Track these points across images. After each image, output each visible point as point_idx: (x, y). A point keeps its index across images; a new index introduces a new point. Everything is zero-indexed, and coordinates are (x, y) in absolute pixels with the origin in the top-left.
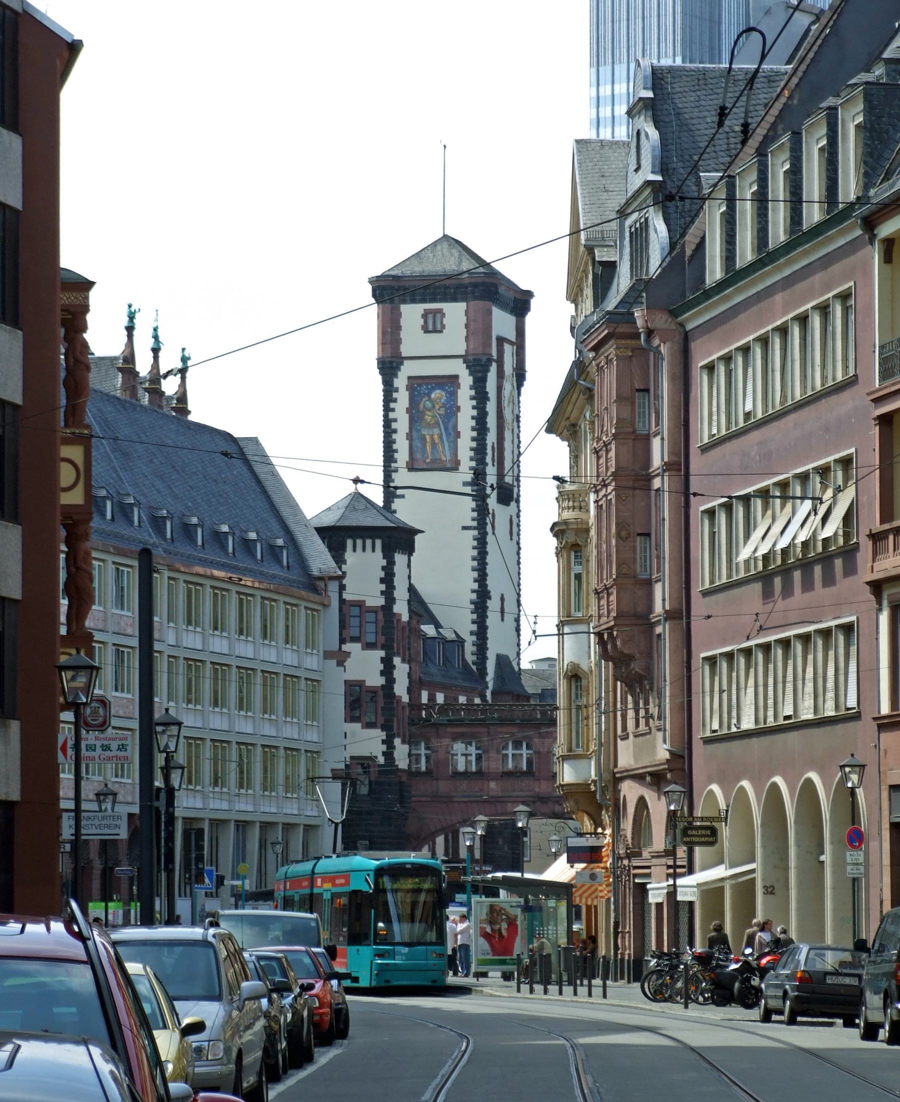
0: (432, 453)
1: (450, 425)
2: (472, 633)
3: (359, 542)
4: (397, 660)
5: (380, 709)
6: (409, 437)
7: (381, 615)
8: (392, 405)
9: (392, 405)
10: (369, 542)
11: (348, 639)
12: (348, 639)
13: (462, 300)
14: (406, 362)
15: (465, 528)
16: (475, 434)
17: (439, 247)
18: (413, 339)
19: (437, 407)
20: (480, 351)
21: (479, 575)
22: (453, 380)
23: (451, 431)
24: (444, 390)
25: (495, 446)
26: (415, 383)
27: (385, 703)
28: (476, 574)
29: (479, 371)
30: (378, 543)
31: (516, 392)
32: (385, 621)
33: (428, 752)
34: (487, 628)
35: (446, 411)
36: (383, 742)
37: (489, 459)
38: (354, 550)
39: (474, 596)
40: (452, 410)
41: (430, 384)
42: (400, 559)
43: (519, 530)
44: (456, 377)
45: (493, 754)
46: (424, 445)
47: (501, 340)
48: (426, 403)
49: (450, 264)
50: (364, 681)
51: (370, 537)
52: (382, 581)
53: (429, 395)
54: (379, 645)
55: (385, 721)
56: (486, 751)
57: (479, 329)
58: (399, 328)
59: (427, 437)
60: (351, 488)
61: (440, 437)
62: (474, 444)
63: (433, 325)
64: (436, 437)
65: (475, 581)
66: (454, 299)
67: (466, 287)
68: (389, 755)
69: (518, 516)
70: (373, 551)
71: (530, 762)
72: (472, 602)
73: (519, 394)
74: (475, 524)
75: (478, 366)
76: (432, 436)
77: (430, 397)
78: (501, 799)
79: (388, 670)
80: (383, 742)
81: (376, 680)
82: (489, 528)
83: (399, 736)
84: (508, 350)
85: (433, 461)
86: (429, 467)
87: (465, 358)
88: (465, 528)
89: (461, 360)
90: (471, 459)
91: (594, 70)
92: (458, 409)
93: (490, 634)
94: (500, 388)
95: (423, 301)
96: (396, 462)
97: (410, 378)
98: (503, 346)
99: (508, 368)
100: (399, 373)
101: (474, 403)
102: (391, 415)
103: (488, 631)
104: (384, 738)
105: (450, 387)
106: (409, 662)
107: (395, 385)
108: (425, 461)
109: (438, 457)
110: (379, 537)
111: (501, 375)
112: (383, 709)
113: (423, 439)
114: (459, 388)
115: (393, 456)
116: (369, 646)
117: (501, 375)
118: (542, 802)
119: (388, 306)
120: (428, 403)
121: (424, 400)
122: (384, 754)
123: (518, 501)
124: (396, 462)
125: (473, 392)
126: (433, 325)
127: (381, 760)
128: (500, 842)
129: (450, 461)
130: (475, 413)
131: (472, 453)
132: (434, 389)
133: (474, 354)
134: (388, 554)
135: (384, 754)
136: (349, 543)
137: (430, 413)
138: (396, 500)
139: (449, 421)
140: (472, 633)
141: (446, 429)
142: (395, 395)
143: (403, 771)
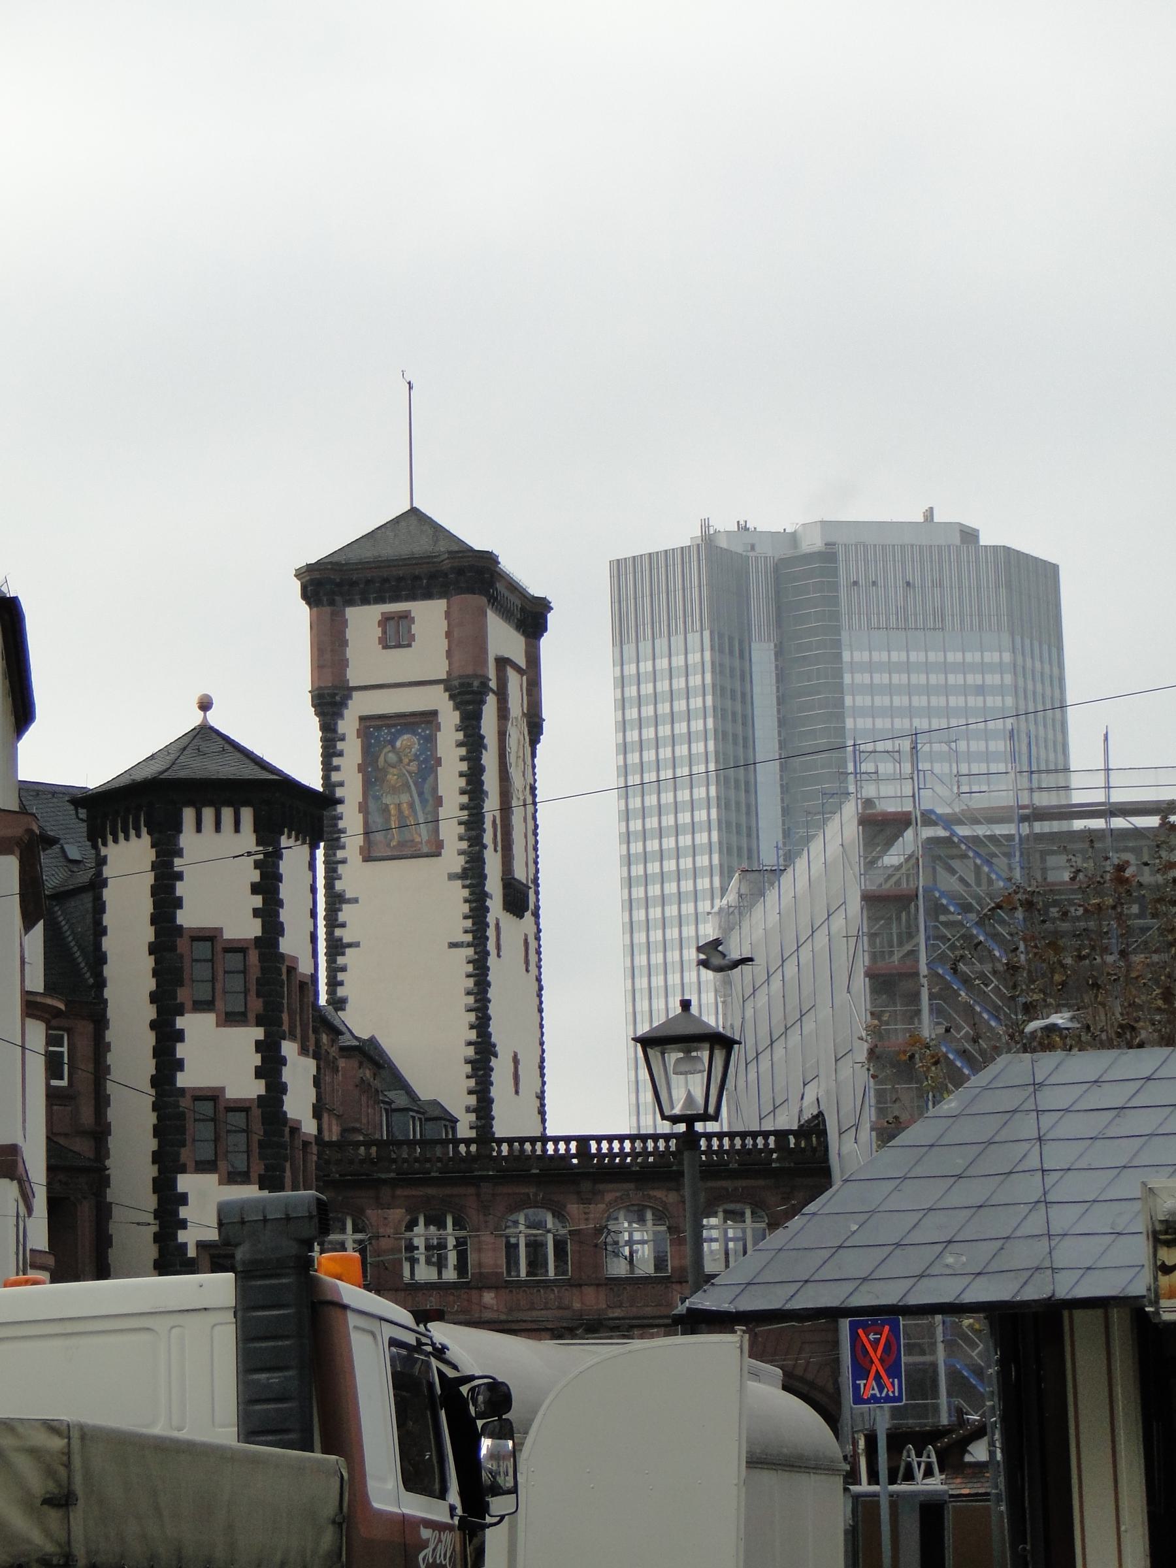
1: (427, 788)
2: (468, 1110)
4: (289, 1049)
5: (255, 1146)
6: (363, 808)
7: (253, 957)
8: (336, 761)
9: (336, 761)
11: (189, 1005)
12: (189, 1005)
13: (441, 596)
14: (355, 694)
15: (453, 945)
16: (465, 799)
17: (403, 524)
18: (366, 657)
19: (406, 761)
20: (469, 671)
21: (477, 1018)
22: (429, 718)
23: (428, 796)
24: (414, 733)
25: (498, 821)
26: (371, 725)
28: (472, 1017)
29: (468, 703)
30: (247, 814)
31: (528, 750)
32: (262, 969)
33: (359, 1236)
34: (491, 1101)
35: (419, 765)
37: (488, 838)
38: (199, 829)
39: (470, 1052)
40: (429, 764)
41: (395, 726)
42: (294, 856)
43: (540, 960)
44: (434, 713)
48: (387, 756)
49: (421, 546)
50: (223, 1089)
51: (229, 804)
52: (255, 889)
53: (392, 743)
55: (267, 1168)
57: (466, 640)
58: (344, 643)
60: (194, 718)
61: (412, 805)
63: (396, 634)
65: (472, 1027)
66: (428, 596)
67: (446, 575)
69: (538, 939)
70: (237, 830)
73: (534, 755)
75: (468, 695)
77: (393, 747)
79: (270, 1066)
81: (245, 1086)
82: (491, 945)
84: (515, 684)
85: (402, 844)
87: (447, 684)
88: (453, 945)
91: (618, 649)
92: (439, 761)
93: (496, 1110)
94: (502, 735)
95: (380, 600)
97: (362, 719)
98: (505, 671)
101: (463, 751)
102: (335, 777)
103: (494, 1106)
105: (424, 730)
106: (316, 1056)
108: (388, 845)
110: (246, 804)
111: (503, 713)
113: (385, 810)
114: (439, 730)
116: (231, 1019)
117: (503, 713)
119: (328, 609)
120: (390, 755)
121: (385, 750)
123: (536, 915)
125: (460, 736)
126: (396, 634)
129: (428, 842)
130: (464, 767)
132: (400, 733)
133: (460, 677)
134: (267, 833)
136: (188, 814)
137: (395, 771)
138: (344, 906)
139: (424, 780)
140: (468, 1110)
141: (421, 794)
142: (340, 746)
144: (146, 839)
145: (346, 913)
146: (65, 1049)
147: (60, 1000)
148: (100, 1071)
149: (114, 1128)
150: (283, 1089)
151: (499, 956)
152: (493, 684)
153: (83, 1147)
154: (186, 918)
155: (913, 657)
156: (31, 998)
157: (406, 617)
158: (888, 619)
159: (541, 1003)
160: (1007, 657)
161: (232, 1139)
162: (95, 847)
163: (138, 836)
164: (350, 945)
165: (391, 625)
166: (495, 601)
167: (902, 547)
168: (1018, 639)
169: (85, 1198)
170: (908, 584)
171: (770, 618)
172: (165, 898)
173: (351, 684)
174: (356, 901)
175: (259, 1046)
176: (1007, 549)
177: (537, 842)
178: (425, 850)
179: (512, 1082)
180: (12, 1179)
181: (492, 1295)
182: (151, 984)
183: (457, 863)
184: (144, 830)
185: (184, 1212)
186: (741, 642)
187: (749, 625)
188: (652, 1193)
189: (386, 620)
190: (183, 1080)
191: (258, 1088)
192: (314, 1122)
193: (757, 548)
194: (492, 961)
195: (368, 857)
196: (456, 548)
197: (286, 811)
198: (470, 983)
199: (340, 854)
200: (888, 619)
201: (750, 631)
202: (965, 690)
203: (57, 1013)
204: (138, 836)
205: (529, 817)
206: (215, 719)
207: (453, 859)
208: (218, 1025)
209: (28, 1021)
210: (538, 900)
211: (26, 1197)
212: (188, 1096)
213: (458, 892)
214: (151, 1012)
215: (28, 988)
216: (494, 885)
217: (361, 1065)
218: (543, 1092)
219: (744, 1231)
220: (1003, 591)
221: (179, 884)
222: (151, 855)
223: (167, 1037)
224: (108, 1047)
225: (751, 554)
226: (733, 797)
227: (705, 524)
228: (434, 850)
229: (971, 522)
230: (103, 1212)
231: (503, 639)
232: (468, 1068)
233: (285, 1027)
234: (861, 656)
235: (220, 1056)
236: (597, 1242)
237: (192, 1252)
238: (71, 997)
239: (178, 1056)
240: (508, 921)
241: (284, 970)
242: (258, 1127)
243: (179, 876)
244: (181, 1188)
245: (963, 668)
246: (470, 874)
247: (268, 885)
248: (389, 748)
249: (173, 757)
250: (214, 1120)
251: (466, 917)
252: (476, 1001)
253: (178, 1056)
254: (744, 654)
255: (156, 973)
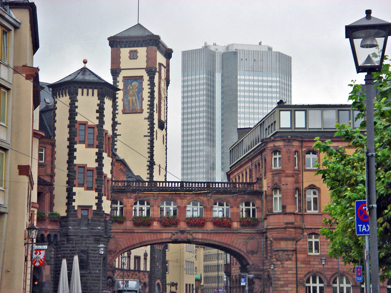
0: (132, 107)
1: (140, 95)
3: (85, 90)
4: (105, 155)
6: (123, 100)
7: (96, 129)
10: (90, 91)
11: (78, 142)
12: (78, 142)
14: (122, 71)
15: (145, 136)
16: (149, 99)
19: (135, 88)
21: (150, 155)
22: (141, 78)
23: (140, 98)
26: (125, 78)
27: (97, 177)
28: (149, 155)
30: (96, 91)
36: (96, 198)
37: (155, 109)
39: (148, 163)
40: (141, 89)
41: (132, 79)
44: (142, 76)
45: (155, 208)
46: (129, 104)
47: (160, 64)
50: (87, 165)
51: (91, 88)
54: (95, 146)
55: (98, 186)
56: (152, 206)
57: (151, 58)
59: (130, 100)
60: (82, 65)
61: (136, 100)
62: (149, 103)
63: (133, 56)
64: (134, 100)
66: (142, 46)
68: (99, 204)
69: (166, 136)
70: (93, 95)
71: (175, 212)
72: (147, 166)
73: (167, 89)
74: (149, 134)
75: (151, 72)
76: (132, 100)
77: (132, 85)
78: (160, 231)
79: (100, 159)
80: (96, 198)
82: (155, 137)
83: (105, 195)
84: (163, 70)
86: (131, 112)
88: (145, 136)
89: (144, 70)
90: (148, 109)
92: (143, 89)
94: (160, 83)
96: (118, 110)
97: (124, 77)
99: (163, 76)
100: (119, 75)
101: (149, 87)
104: (97, 196)
105: (140, 81)
107: (118, 80)
108: (129, 110)
109: (134, 108)
110: (96, 88)
111: (160, 78)
112: (96, 180)
113: (129, 101)
115: (116, 108)
116: (89, 146)
117: (160, 78)
118: (181, 233)
120: (131, 87)
122: (96, 204)
123: (166, 130)
124: (118, 110)
126: (133, 56)
127: (95, 208)
128: (158, 264)
130: (149, 90)
131: (148, 107)
134: (101, 97)
135: (96, 204)
136: (80, 91)
137: (132, 91)
138: (117, 125)
139: (139, 94)
141: (138, 97)
143: (107, 215)
144: (68, 97)
145: (118, 127)
146: (43, 153)
147: (43, 132)
148: (53, 158)
149: (55, 205)
150: (103, 165)
151: (156, 139)
152: (158, 70)
153: (48, 179)
154: (78, 118)
155: (255, 78)
156: (35, 132)
157: (136, 51)
158: (249, 69)
159: (166, 152)
160: (278, 79)
161: (88, 178)
162: (54, 98)
163: (66, 96)
164: (118, 135)
165: (132, 53)
166: (159, 48)
167: (254, 51)
168: (281, 75)
169: (47, 193)
170: (255, 60)
171: (222, 66)
172: (73, 113)
173: (121, 68)
174: (120, 124)
175: (97, 154)
176: (279, 53)
177: (167, 111)
178: (139, 111)
179: (159, 172)
180: (27, 176)
181: (156, 223)
182: (68, 136)
183: (147, 115)
184: (67, 94)
185: (74, 197)
186: (213, 73)
187: (215, 69)
188: (200, 197)
189: (131, 52)
190: (75, 162)
191: (96, 165)
192: (111, 175)
193: (218, 50)
194: (155, 141)
195: (124, 112)
196: (149, 34)
197: (106, 91)
198: (149, 146)
199: (117, 112)
200: (249, 69)
201: (215, 70)
202: (267, 87)
203: (42, 137)
204: (66, 96)
205: (165, 105)
206: (88, 66)
207: (146, 114)
208: (86, 148)
209: (34, 138)
210: (167, 126)
211: (31, 183)
212: (77, 166)
213: (147, 123)
214: (68, 143)
215: (34, 129)
216: (156, 121)
217: (121, 165)
218: (166, 175)
219: (223, 209)
220: (278, 63)
221: (76, 109)
222: (69, 101)
223: (72, 151)
224: (55, 159)
225: (216, 51)
226: (210, 111)
227: (206, 43)
228: (141, 112)
229: (270, 45)
230: (52, 197)
231: (161, 59)
232: (148, 168)
233: (104, 149)
234: (242, 77)
235: (86, 156)
236: (184, 209)
237: (76, 208)
238: (45, 134)
239: (75, 155)
240: (159, 131)
241: (104, 133)
242: (96, 177)
243: (77, 107)
244: (74, 191)
245: (267, 81)
246: (150, 118)
247: (101, 110)
248: (130, 85)
249: (76, 75)
250: (84, 173)
251: (148, 129)
252: (150, 151)
253: (75, 155)
254: (214, 76)
255: (69, 133)
